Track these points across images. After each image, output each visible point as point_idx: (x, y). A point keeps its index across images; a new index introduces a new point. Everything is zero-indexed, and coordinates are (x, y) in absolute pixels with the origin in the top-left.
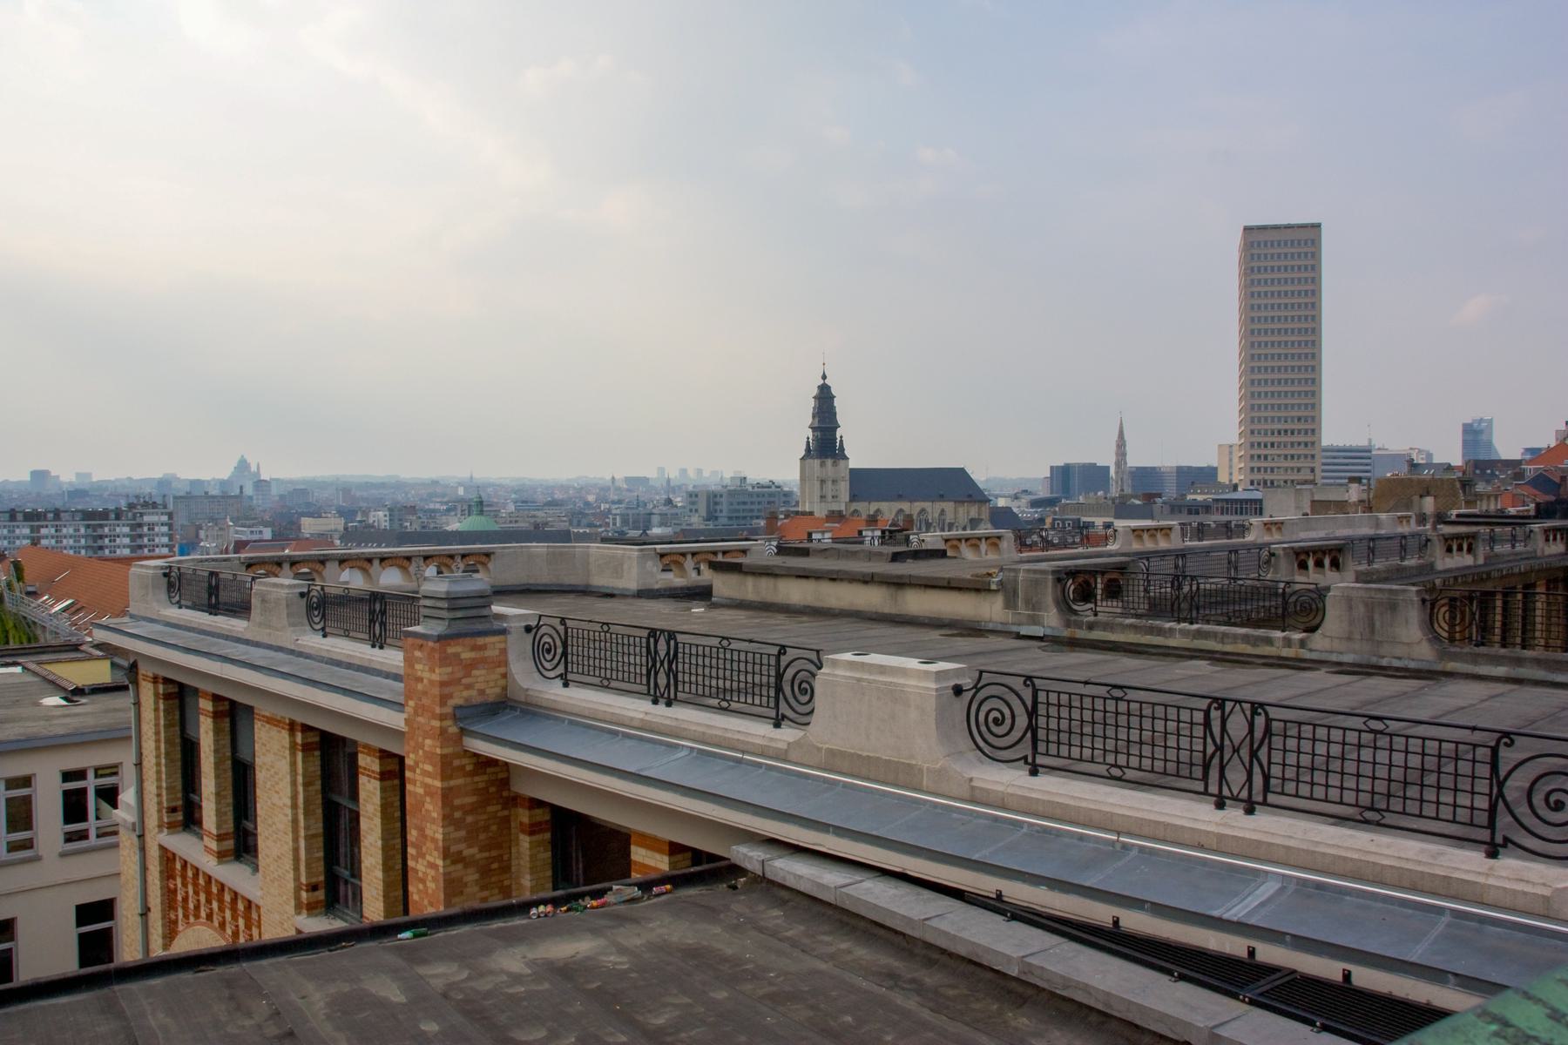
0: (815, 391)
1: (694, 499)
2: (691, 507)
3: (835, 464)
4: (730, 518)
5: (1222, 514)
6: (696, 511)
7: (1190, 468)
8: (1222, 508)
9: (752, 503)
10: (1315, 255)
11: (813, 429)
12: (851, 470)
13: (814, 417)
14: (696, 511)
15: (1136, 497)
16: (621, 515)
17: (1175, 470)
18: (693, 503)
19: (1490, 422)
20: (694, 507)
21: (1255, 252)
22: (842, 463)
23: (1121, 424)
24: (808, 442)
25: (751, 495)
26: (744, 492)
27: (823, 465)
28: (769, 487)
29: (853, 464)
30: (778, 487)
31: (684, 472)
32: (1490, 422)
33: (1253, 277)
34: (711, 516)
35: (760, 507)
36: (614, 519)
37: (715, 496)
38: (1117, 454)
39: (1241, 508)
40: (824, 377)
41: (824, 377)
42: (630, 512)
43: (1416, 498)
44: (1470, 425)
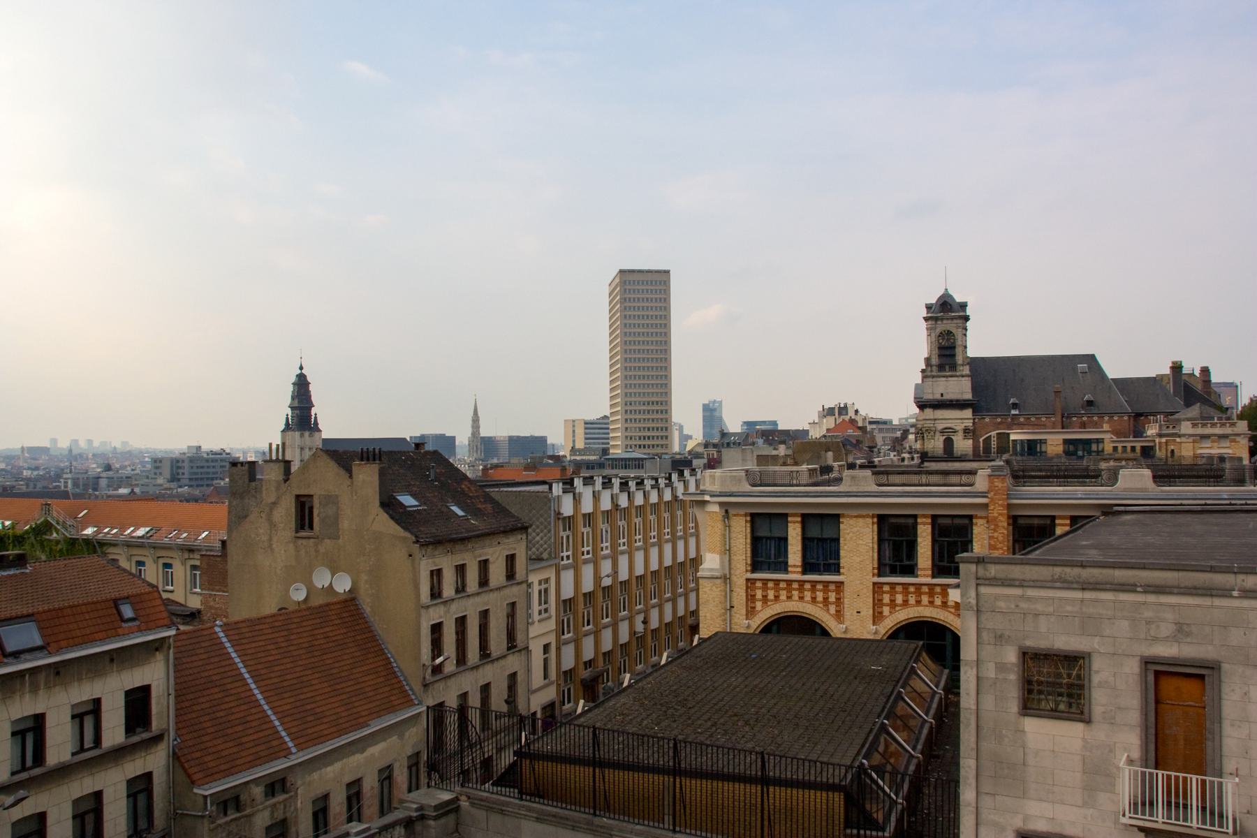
0: (293, 379)
1: (158, 464)
2: (156, 471)
3: (311, 435)
4: (191, 479)
5: (613, 468)
6: (161, 474)
7: (518, 437)
8: (612, 464)
9: (208, 467)
10: (667, 291)
11: (292, 408)
12: (323, 439)
13: (293, 398)
14: (161, 474)
15: (98, 468)
16: (73, 479)
17: (507, 439)
18: (157, 468)
19: (720, 403)
20: (158, 471)
21: (628, 287)
22: (317, 433)
23: (476, 404)
24: (287, 419)
25: (207, 461)
26: (201, 459)
27: (302, 436)
28: (221, 454)
29: (325, 435)
30: (229, 454)
31: (90, 442)
32: (720, 403)
33: (625, 305)
34: (174, 478)
35: (214, 470)
36: (66, 483)
37: (178, 461)
38: (473, 427)
39: (626, 465)
40: (301, 368)
41: (301, 368)
42: (80, 476)
43: (823, 453)
44: (708, 405)
